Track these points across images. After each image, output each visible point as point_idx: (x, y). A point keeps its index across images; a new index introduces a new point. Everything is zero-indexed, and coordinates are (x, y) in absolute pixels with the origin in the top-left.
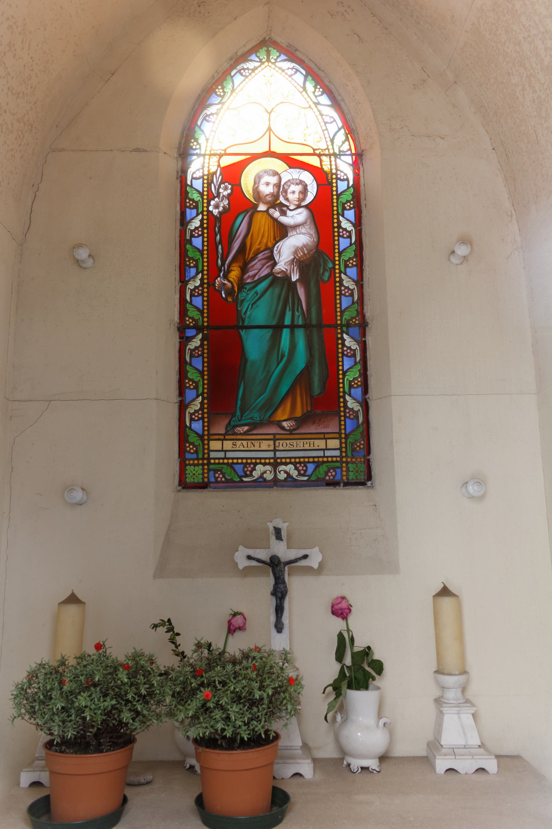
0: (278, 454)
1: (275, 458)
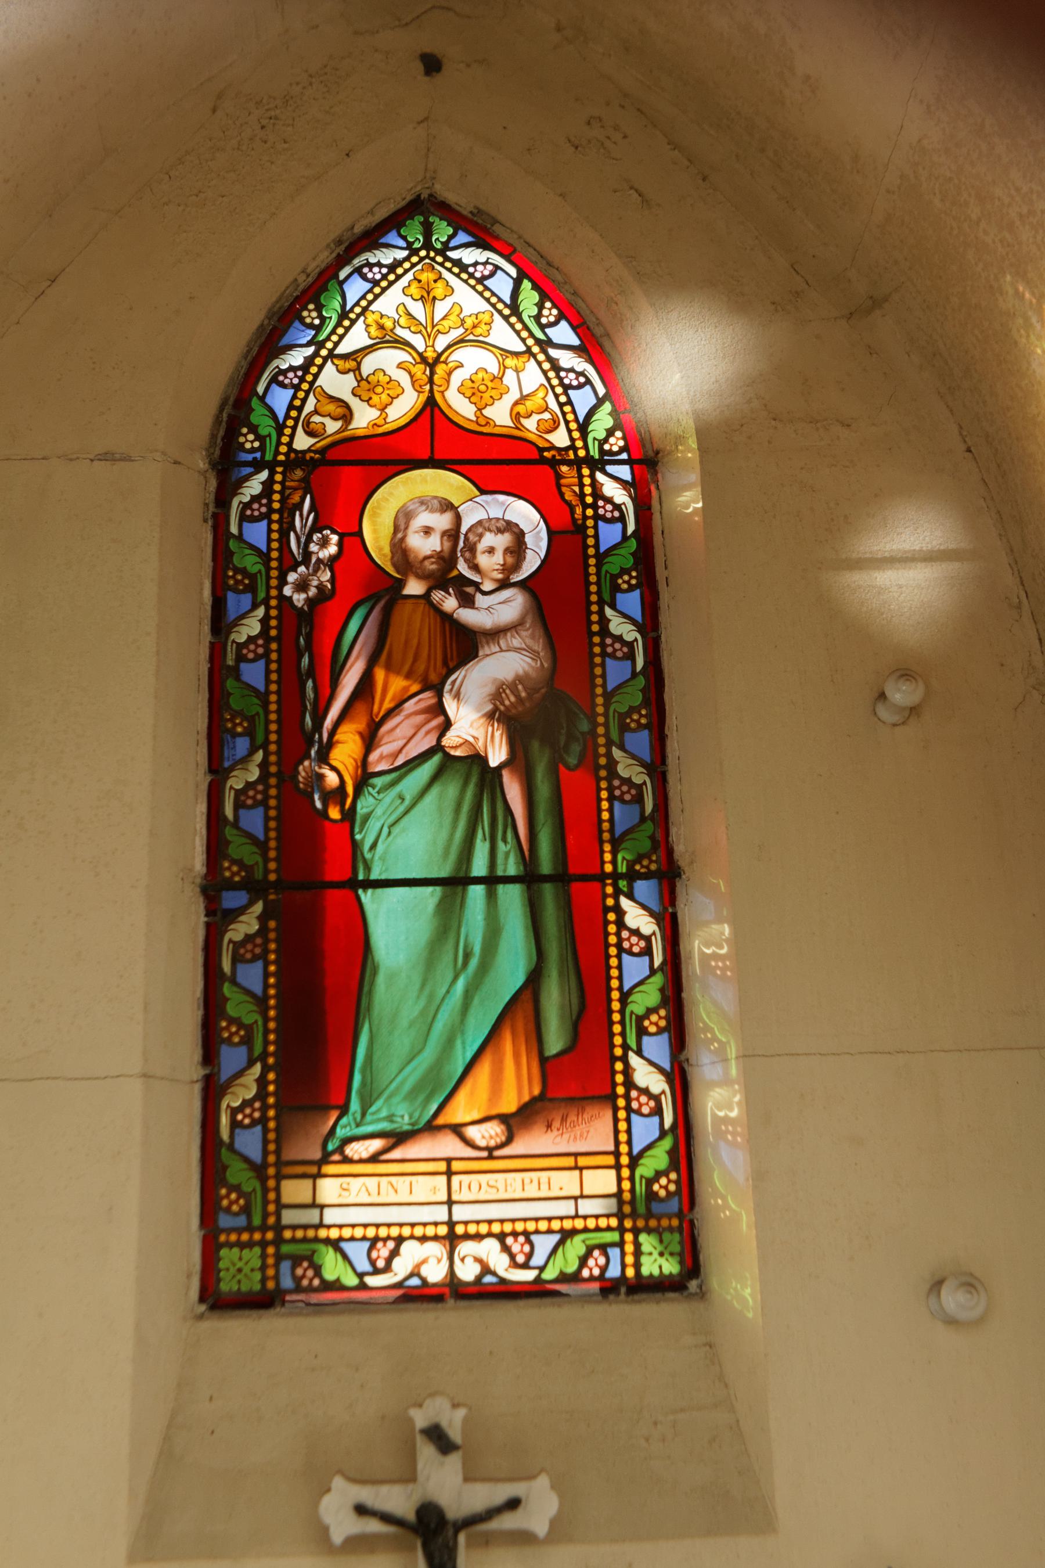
0: (460, 1213)
1: (451, 1224)
